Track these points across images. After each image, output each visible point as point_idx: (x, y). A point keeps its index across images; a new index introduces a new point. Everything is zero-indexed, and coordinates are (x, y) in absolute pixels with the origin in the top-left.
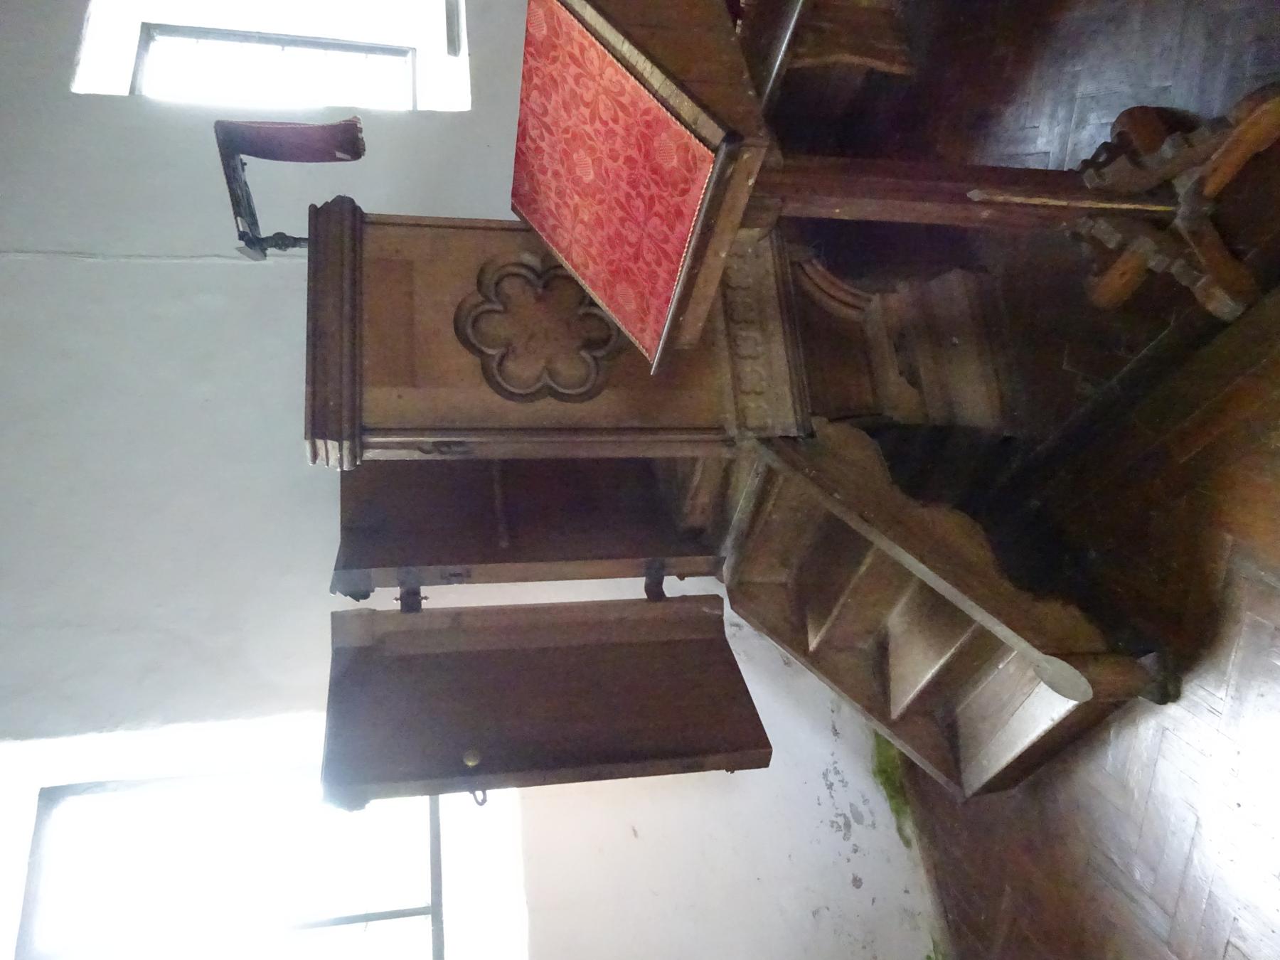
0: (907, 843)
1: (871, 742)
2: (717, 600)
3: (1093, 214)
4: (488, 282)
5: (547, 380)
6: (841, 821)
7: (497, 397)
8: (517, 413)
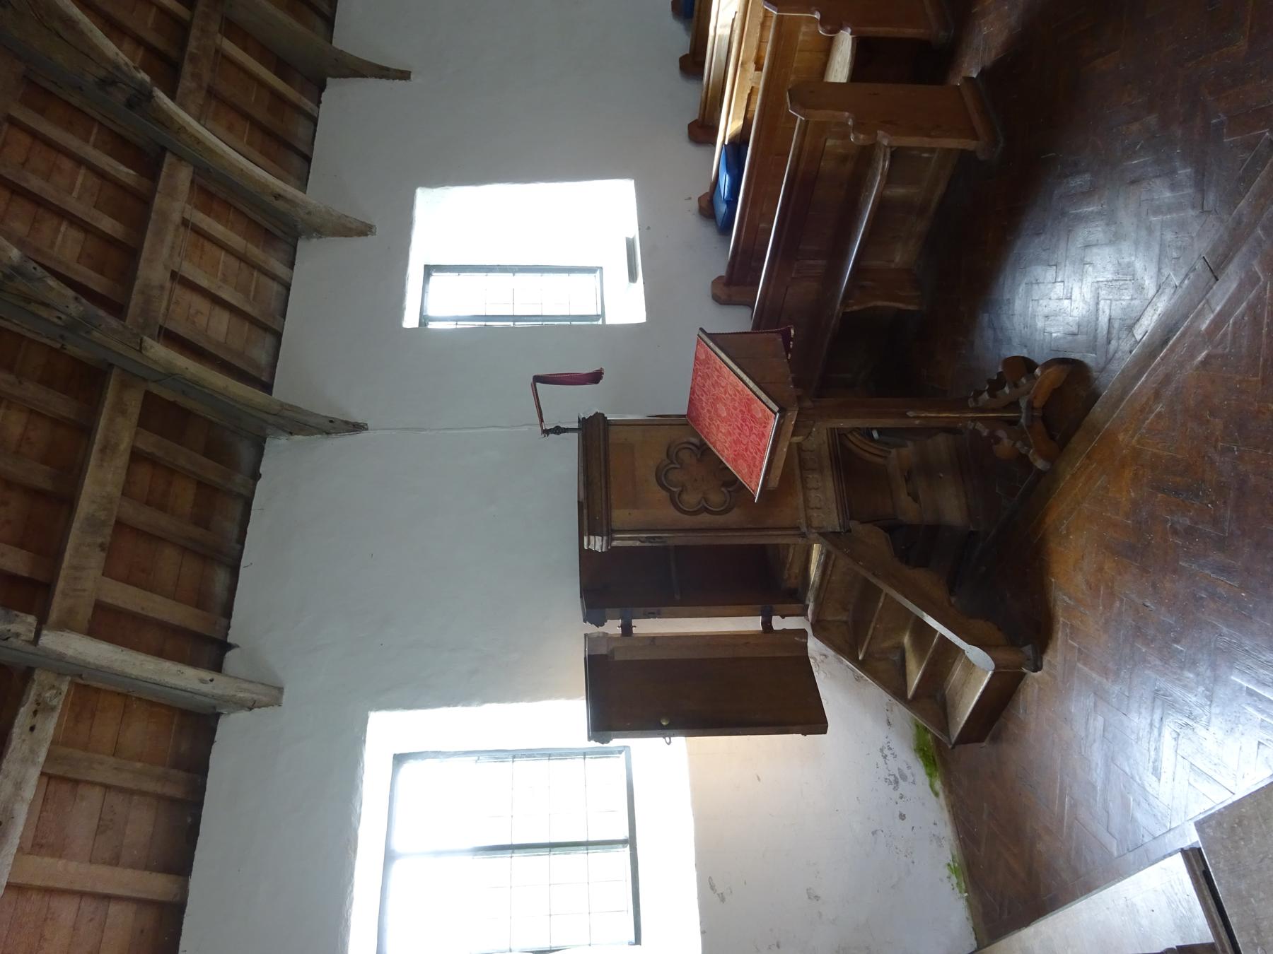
0: (937, 795)
1: (914, 727)
2: (803, 633)
3: (974, 420)
4: (672, 453)
5: (703, 502)
6: (892, 778)
7: (678, 514)
8: (688, 521)
